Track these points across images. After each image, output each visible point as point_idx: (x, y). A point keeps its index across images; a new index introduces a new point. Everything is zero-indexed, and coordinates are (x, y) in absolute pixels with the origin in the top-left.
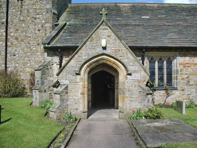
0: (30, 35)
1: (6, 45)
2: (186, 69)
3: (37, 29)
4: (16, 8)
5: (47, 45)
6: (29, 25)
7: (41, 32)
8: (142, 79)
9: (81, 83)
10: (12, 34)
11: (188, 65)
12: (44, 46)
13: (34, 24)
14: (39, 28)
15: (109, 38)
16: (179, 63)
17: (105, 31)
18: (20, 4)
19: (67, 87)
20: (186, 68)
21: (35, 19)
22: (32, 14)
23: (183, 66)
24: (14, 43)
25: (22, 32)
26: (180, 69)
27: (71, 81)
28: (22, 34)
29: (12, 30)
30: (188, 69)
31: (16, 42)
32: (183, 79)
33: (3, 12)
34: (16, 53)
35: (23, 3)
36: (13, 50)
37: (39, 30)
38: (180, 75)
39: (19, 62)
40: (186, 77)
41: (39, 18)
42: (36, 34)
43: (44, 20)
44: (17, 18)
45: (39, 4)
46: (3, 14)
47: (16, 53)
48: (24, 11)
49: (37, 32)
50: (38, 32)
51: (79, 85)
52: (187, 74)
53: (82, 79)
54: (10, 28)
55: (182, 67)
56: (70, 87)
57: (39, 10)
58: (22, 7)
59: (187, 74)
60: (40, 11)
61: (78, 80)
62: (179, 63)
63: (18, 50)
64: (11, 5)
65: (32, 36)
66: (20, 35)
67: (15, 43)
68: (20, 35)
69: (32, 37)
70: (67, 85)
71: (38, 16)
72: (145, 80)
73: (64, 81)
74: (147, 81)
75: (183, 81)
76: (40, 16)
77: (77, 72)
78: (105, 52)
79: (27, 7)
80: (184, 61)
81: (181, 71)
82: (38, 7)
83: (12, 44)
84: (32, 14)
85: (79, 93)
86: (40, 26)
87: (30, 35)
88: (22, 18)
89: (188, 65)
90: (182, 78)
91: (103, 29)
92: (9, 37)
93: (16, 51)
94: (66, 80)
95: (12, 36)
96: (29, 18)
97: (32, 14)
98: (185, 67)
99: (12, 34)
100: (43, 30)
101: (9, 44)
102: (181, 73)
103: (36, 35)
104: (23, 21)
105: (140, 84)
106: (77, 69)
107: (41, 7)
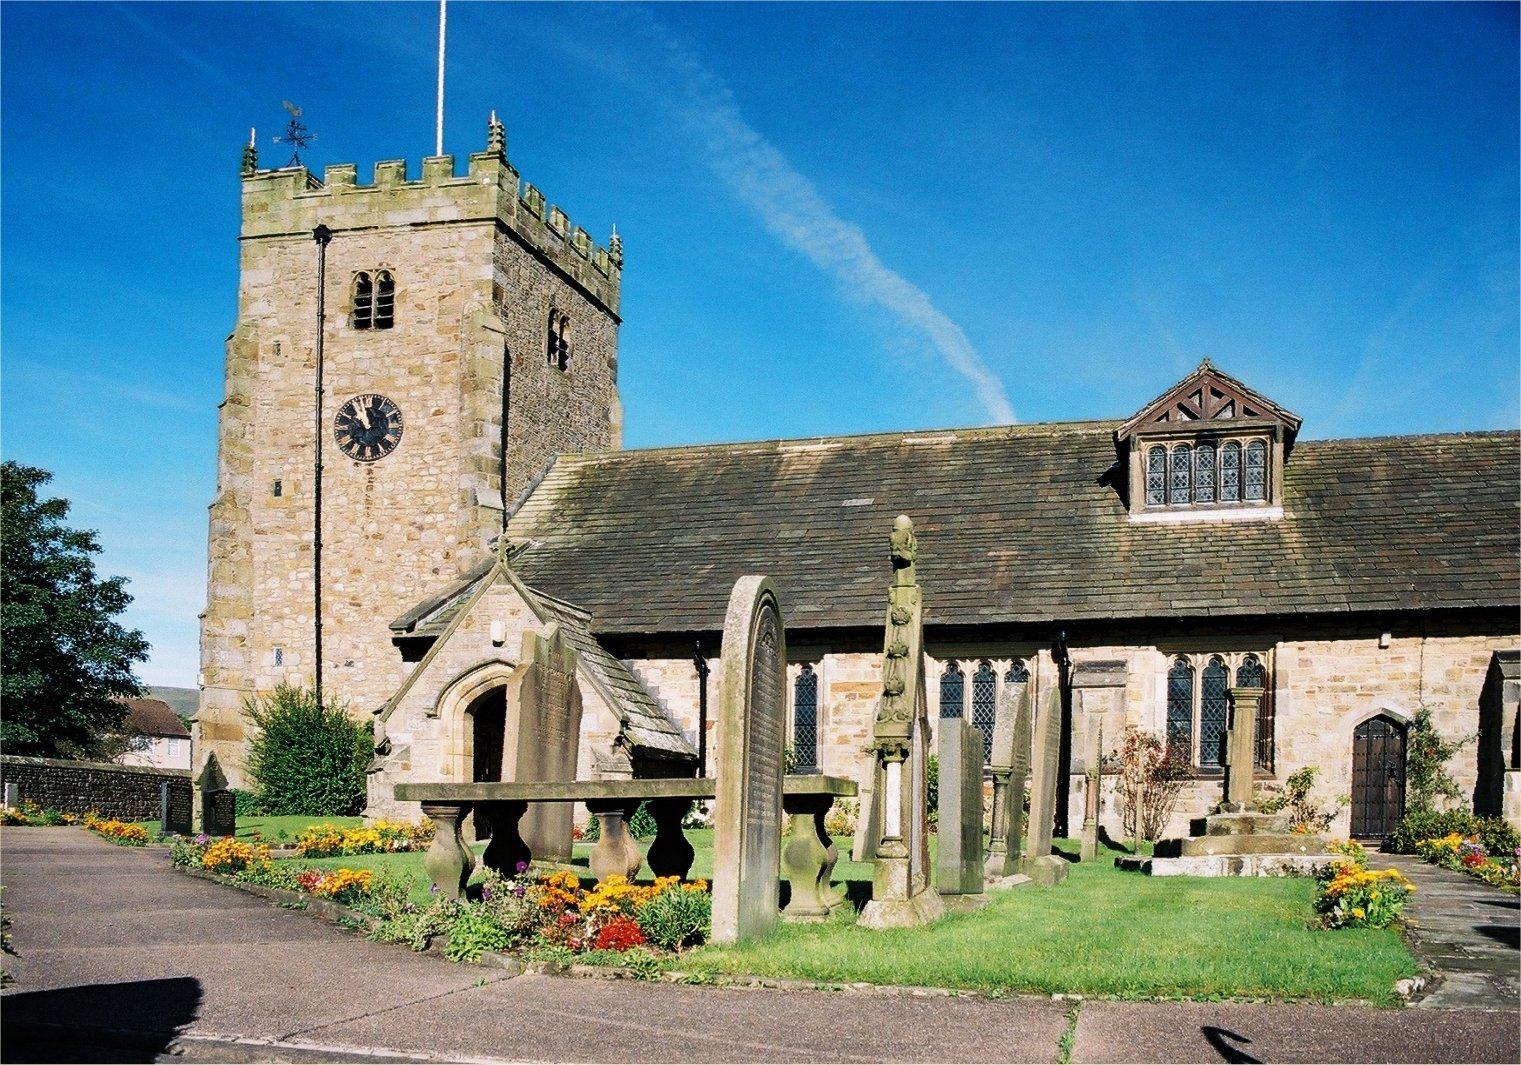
0: (403, 589)
1: (319, 626)
2: (855, 706)
3: (430, 565)
4: (352, 490)
5: (405, 634)
6: (399, 551)
7: (442, 578)
8: (603, 731)
9: (444, 742)
10: (339, 587)
11: (863, 690)
12: (397, 636)
13: (418, 549)
14: (433, 562)
15: (513, 619)
16: (833, 685)
17: (505, 597)
18: (364, 474)
19: (407, 750)
20: (859, 701)
21: (421, 528)
22: (407, 511)
23: (845, 693)
24: (346, 620)
25: (375, 577)
26: (833, 705)
27: (418, 736)
28: (375, 586)
29: (339, 573)
30: (864, 705)
31: (352, 616)
32: (843, 740)
33: (304, 508)
34: (357, 654)
35: (375, 470)
36: (346, 645)
37: (435, 571)
38: (836, 726)
39: (366, 689)
40: (858, 732)
41: (433, 526)
42: (424, 584)
43: (454, 533)
44: (353, 527)
45: (433, 475)
46: (303, 513)
47: (357, 654)
48: (377, 501)
49: (428, 577)
50: (434, 578)
51: (436, 748)
52: (859, 722)
53: (444, 731)
54: (332, 564)
55: (841, 696)
56: (414, 751)
57: (433, 496)
58: (370, 488)
59: (859, 722)
60: (438, 499)
61: (435, 734)
62: (833, 685)
63: (361, 646)
64: (331, 480)
65: (410, 594)
66: (368, 590)
67: (351, 619)
68: (368, 590)
69: (413, 597)
70: (408, 748)
71: (429, 519)
72: (609, 733)
73: (400, 735)
74: (615, 736)
75: (843, 748)
76: (440, 517)
77: (431, 712)
78: (500, 653)
79: (389, 487)
80: (849, 676)
81: (837, 710)
82: (431, 486)
83: (340, 621)
84: (412, 513)
85: (439, 769)
86: (438, 556)
87: (403, 589)
88: (372, 528)
89: (863, 690)
90: (840, 738)
91: (499, 593)
92: (325, 597)
93: (355, 647)
94: (406, 731)
95: (340, 594)
96: (397, 527)
97: (412, 513)
98: (851, 697)
99: (339, 587)
100: (449, 571)
101: (326, 621)
102: (837, 718)
103: (426, 590)
104: (375, 537)
105: (595, 746)
106: (432, 704)
107: (442, 486)
